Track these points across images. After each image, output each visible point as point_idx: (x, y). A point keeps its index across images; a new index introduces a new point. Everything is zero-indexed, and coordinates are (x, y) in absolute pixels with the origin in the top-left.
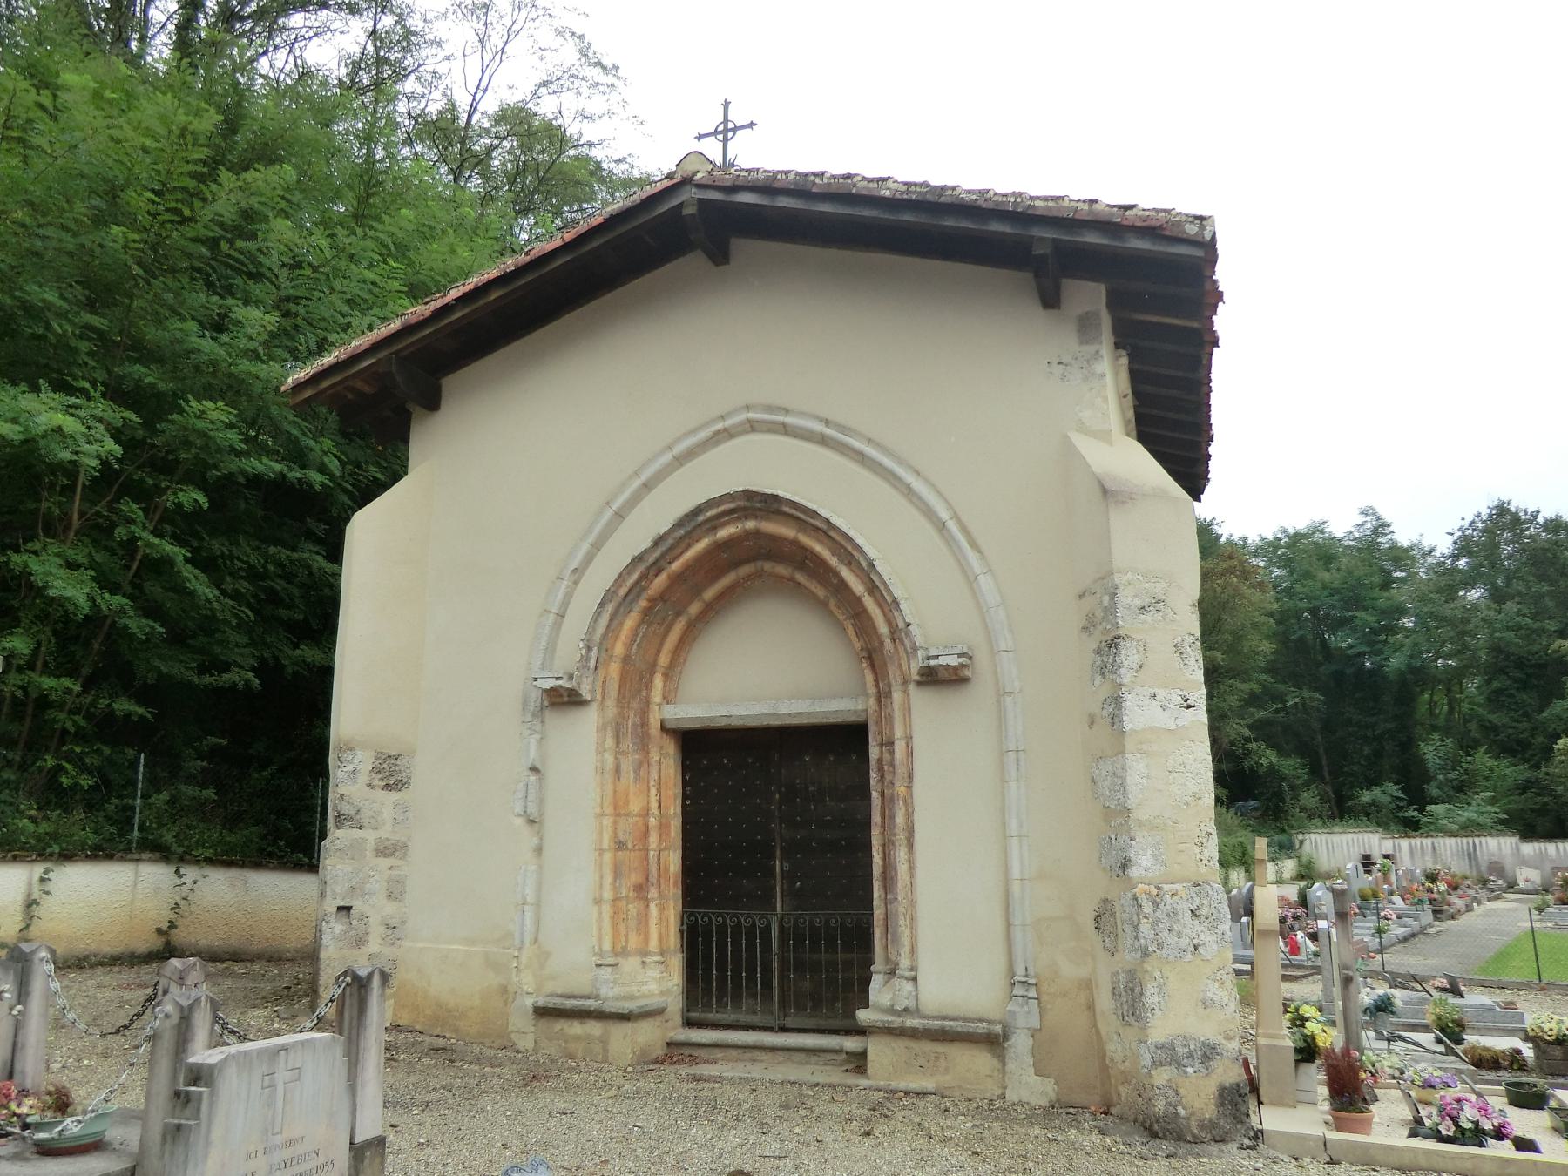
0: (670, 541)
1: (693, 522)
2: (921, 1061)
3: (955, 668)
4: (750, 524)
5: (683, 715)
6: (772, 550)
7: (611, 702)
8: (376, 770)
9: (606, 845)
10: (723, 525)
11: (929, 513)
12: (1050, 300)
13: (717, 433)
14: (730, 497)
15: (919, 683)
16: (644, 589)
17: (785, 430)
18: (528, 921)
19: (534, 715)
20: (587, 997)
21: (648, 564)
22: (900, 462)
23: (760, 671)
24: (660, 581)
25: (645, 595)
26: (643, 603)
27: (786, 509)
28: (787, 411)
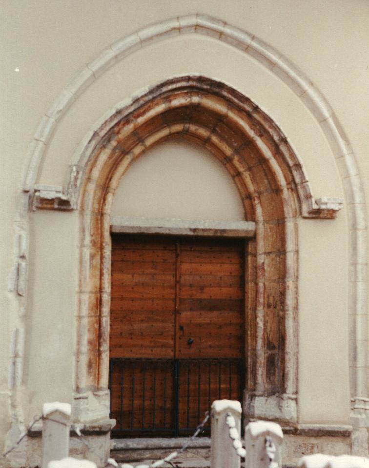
0: (142, 102)
1: (161, 92)
2: (303, 450)
4: (196, 99)
6: (218, 122)
10: (176, 96)
11: (315, 109)
13: (174, 29)
16: (118, 133)
17: (221, 35)
23: (183, 193)
26: (114, 143)
27: (225, 93)
28: (225, 24)
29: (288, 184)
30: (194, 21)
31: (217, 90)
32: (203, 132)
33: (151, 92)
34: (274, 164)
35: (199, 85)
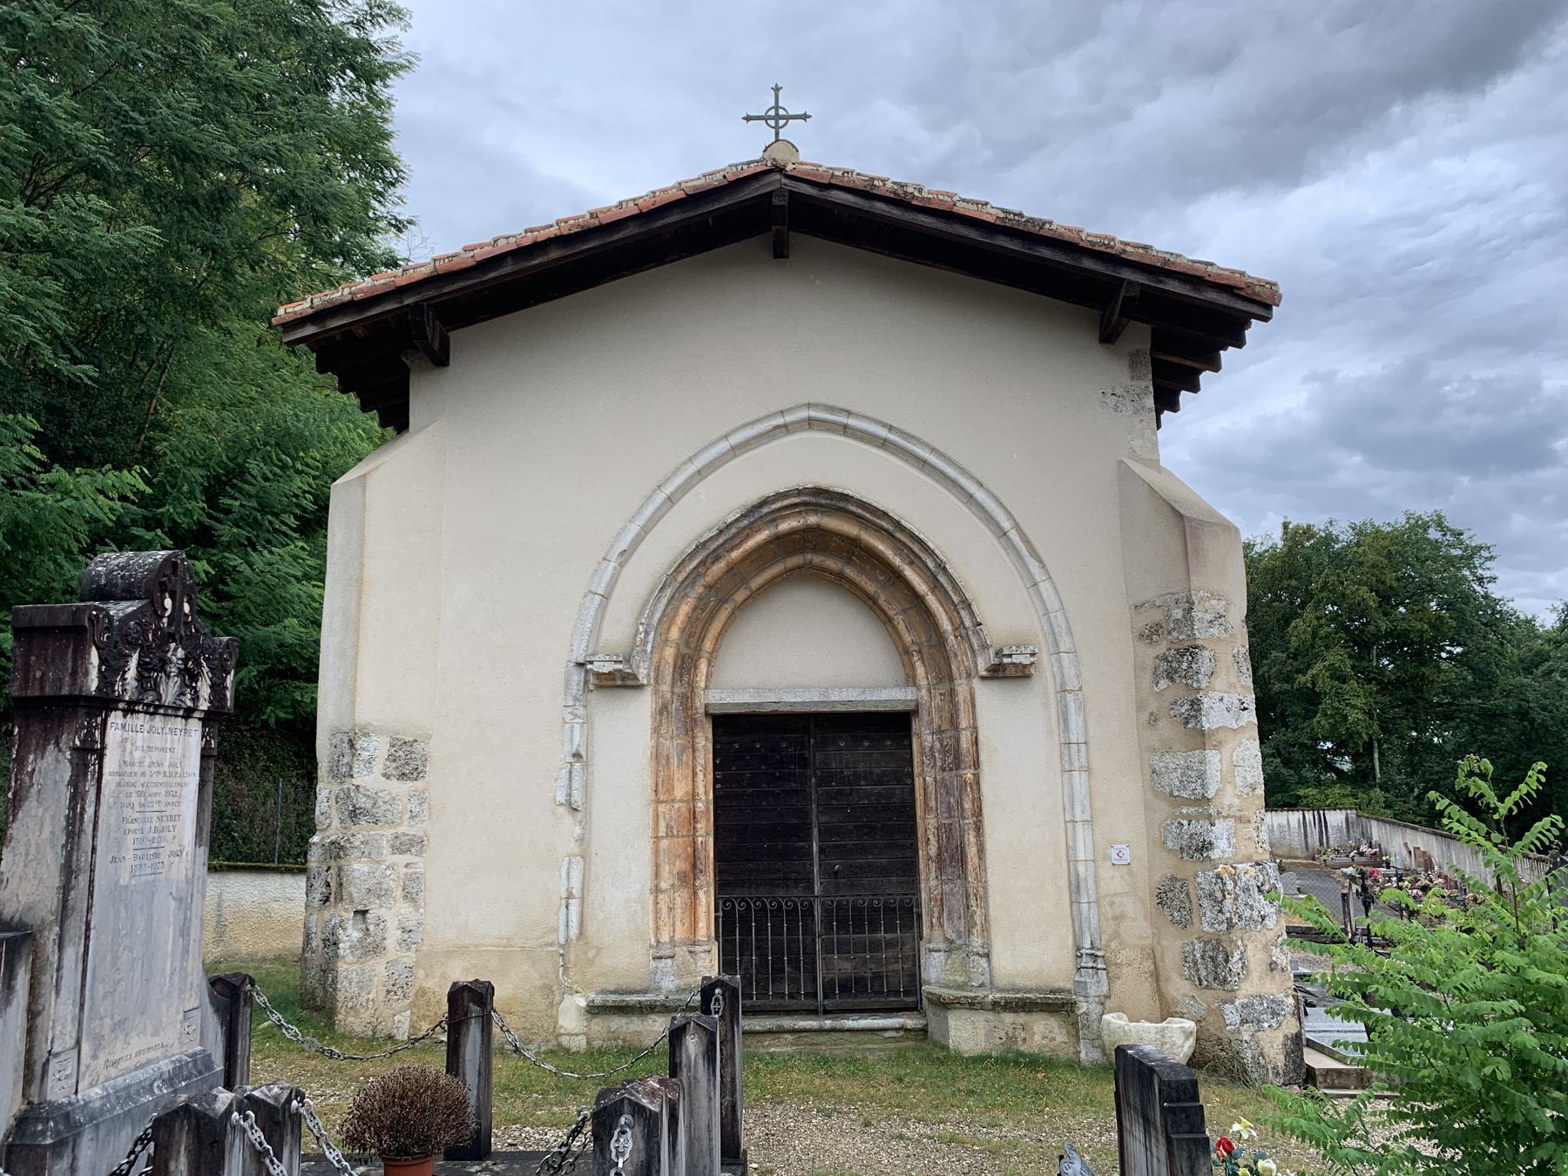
1: (758, 513)
3: (1025, 666)
4: (813, 519)
5: (729, 700)
7: (666, 688)
8: (392, 758)
9: (662, 833)
10: (784, 518)
11: (989, 519)
12: (1108, 337)
13: (778, 427)
14: (799, 492)
15: (983, 678)
16: (704, 575)
17: (845, 430)
18: (574, 918)
19: (576, 699)
20: (645, 992)
21: (708, 551)
22: (963, 471)
23: (808, 657)
24: (720, 567)
25: (702, 582)
27: (853, 508)
28: (849, 413)
29: (955, 629)
30: (804, 414)
31: (842, 505)
32: (832, 564)
33: (743, 516)
34: (932, 601)
35: (813, 500)
